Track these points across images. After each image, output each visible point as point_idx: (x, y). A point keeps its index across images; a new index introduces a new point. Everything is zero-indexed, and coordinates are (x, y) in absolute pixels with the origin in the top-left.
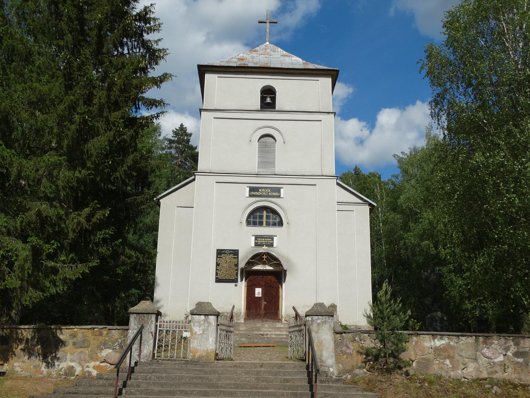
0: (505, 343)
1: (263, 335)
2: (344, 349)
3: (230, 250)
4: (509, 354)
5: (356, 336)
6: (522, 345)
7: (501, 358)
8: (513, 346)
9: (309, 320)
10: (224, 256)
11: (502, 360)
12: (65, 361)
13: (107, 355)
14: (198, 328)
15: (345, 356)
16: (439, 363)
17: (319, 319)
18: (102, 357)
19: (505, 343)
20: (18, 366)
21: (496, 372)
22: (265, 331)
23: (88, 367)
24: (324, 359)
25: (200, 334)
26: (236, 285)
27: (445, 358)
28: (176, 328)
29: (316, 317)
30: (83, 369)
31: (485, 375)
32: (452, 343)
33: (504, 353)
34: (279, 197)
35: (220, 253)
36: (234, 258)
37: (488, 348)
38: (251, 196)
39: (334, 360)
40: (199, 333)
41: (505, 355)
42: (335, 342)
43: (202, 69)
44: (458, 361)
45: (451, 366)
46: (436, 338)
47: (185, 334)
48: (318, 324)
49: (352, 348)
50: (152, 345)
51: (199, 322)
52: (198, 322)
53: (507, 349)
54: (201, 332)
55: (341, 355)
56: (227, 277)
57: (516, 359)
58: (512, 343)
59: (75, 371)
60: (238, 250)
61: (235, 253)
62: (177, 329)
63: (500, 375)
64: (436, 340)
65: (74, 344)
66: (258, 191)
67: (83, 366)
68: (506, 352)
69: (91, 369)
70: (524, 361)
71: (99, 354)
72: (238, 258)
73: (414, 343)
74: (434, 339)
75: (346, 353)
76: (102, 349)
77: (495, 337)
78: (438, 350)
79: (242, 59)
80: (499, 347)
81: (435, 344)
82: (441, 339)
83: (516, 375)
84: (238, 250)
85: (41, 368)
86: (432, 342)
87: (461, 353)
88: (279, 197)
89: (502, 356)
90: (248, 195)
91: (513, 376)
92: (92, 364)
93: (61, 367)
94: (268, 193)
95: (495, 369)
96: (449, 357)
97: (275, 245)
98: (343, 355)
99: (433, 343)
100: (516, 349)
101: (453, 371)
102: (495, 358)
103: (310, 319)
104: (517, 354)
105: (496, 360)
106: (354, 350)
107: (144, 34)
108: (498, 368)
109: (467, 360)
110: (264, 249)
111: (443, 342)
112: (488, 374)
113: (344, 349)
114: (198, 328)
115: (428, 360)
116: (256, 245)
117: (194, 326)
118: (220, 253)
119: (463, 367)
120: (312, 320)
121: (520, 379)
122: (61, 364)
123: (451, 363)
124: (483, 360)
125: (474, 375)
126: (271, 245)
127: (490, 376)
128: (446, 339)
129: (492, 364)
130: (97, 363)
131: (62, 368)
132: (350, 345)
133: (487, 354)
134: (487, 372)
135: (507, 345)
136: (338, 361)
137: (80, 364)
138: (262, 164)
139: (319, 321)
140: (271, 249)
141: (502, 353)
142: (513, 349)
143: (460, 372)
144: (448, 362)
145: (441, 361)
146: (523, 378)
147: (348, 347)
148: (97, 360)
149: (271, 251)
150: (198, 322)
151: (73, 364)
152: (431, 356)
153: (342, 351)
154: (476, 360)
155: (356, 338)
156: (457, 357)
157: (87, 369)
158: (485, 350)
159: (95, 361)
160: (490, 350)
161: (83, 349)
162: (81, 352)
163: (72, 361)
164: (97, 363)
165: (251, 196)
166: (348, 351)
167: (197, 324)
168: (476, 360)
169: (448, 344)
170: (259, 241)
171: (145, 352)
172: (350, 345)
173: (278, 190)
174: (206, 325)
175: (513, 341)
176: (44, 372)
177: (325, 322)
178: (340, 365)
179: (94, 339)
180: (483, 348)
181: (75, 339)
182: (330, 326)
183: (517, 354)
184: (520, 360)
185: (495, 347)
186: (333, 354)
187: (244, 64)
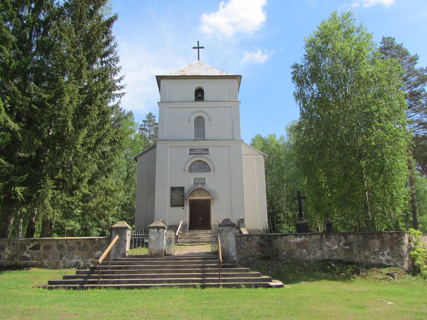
0: (339, 238)
1: (199, 238)
2: (242, 245)
3: (179, 187)
4: (341, 244)
5: (249, 238)
6: (348, 238)
7: (336, 247)
8: (343, 239)
9: (220, 229)
10: (176, 191)
11: (337, 248)
12: (74, 259)
13: (99, 255)
14: (153, 236)
15: (243, 250)
16: (299, 252)
17: (226, 228)
18: (96, 256)
19: (339, 238)
20: (46, 263)
21: (334, 255)
22: (201, 236)
23: (87, 262)
24: (230, 252)
25: (155, 240)
26: (183, 208)
27: (303, 248)
28: (136, 237)
29: (225, 227)
30: (85, 263)
31: (327, 257)
32: (307, 240)
33: (338, 243)
34: (208, 154)
35: (173, 189)
36: (181, 192)
37: (328, 241)
38: (190, 154)
39: (236, 252)
40: (154, 240)
41: (338, 245)
42: (236, 242)
43: (159, 78)
44: (311, 250)
45: (306, 253)
46: (297, 237)
47: (146, 241)
48: (226, 232)
49: (247, 245)
50: (199, 246)
51: (154, 233)
52: (153, 233)
53: (340, 241)
54: (155, 239)
55: (241, 249)
56: (178, 204)
57: (345, 247)
58: (343, 238)
59: (80, 265)
60: (184, 187)
61: (182, 189)
62: (141, 238)
63: (336, 257)
64: (297, 238)
65: (79, 248)
66: (195, 151)
67: (84, 262)
68: (339, 243)
69: (89, 263)
70: (350, 248)
71: (94, 254)
72: (184, 192)
73: (284, 241)
74: (296, 237)
75: (243, 248)
76: (95, 251)
77: (332, 235)
78: (299, 244)
79: (183, 71)
80: (335, 240)
81: (297, 240)
82: (301, 237)
83: (345, 257)
84: (184, 187)
85: (60, 263)
86: (295, 239)
87: (312, 245)
88: (208, 154)
89: (337, 246)
90: (188, 153)
91: (344, 258)
92: (90, 260)
93: (71, 262)
94: (201, 151)
95: (332, 254)
96: (305, 248)
97: (206, 183)
98: (242, 249)
99: (295, 240)
100: (345, 241)
101: (308, 256)
102: (333, 247)
103: (221, 229)
104: (345, 244)
105: (333, 248)
106: (248, 246)
107: (116, 84)
108: (335, 253)
109: (316, 249)
110: (200, 186)
111: (302, 239)
112: (329, 256)
113: (242, 245)
114: (153, 236)
115: (293, 250)
116: (195, 184)
117: (151, 235)
118: (173, 189)
119: (313, 253)
120: (222, 229)
121: (348, 259)
122: (72, 261)
123: (307, 251)
124: (325, 249)
125: (320, 258)
126: (204, 184)
127: (330, 258)
128: (304, 237)
129: (331, 250)
130: (93, 260)
131: (72, 263)
132: (246, 243)
133: (328, 245)
134: (328, 256)
135: (340, 239)
136: (238, 253)
137: (83, 260)
138: (197, 134)
139: (226, 230)
140: (203, 185)
141: (337, 244)
142: (343, 241)
143: (312, 256)
144: (304, 251)
145: (300, 250)
146: (350, 258)
147: (244, 245)
148: (92, 258)
149: (203, 187)
150: (153, 233)
151: (78, 261)
152: (295, 248)
153: (241, 247)
154: (321, 249)
155: (249, 239)
156: (310, 247)
157: (87, 263)
158: (327, 243)
159: (92, 258)
160: (330, 242)
161: (84, 251)
162: (84, 253)
163: (78, 259)
164: (93, 260)
165: (190, 154)
166: (245, 247)
167: (152, 234)
168: (321, 249)
169: (305, 240)
170: (197, 181)
171: (122, 252)
172: (246, 243)
173: (207, 150)
174: (158, 235)
175: (343, 237)
176: (62, 266)
177: (230, 230)
178: (240, 256)
179: (91, 245)
180: (325, 242)
181: (79, 246)
182: (233, 232)
183: (345, 244)
184: (348, 247)
185: (333, 240)
186: (236, 249)
187: (184, 74)
